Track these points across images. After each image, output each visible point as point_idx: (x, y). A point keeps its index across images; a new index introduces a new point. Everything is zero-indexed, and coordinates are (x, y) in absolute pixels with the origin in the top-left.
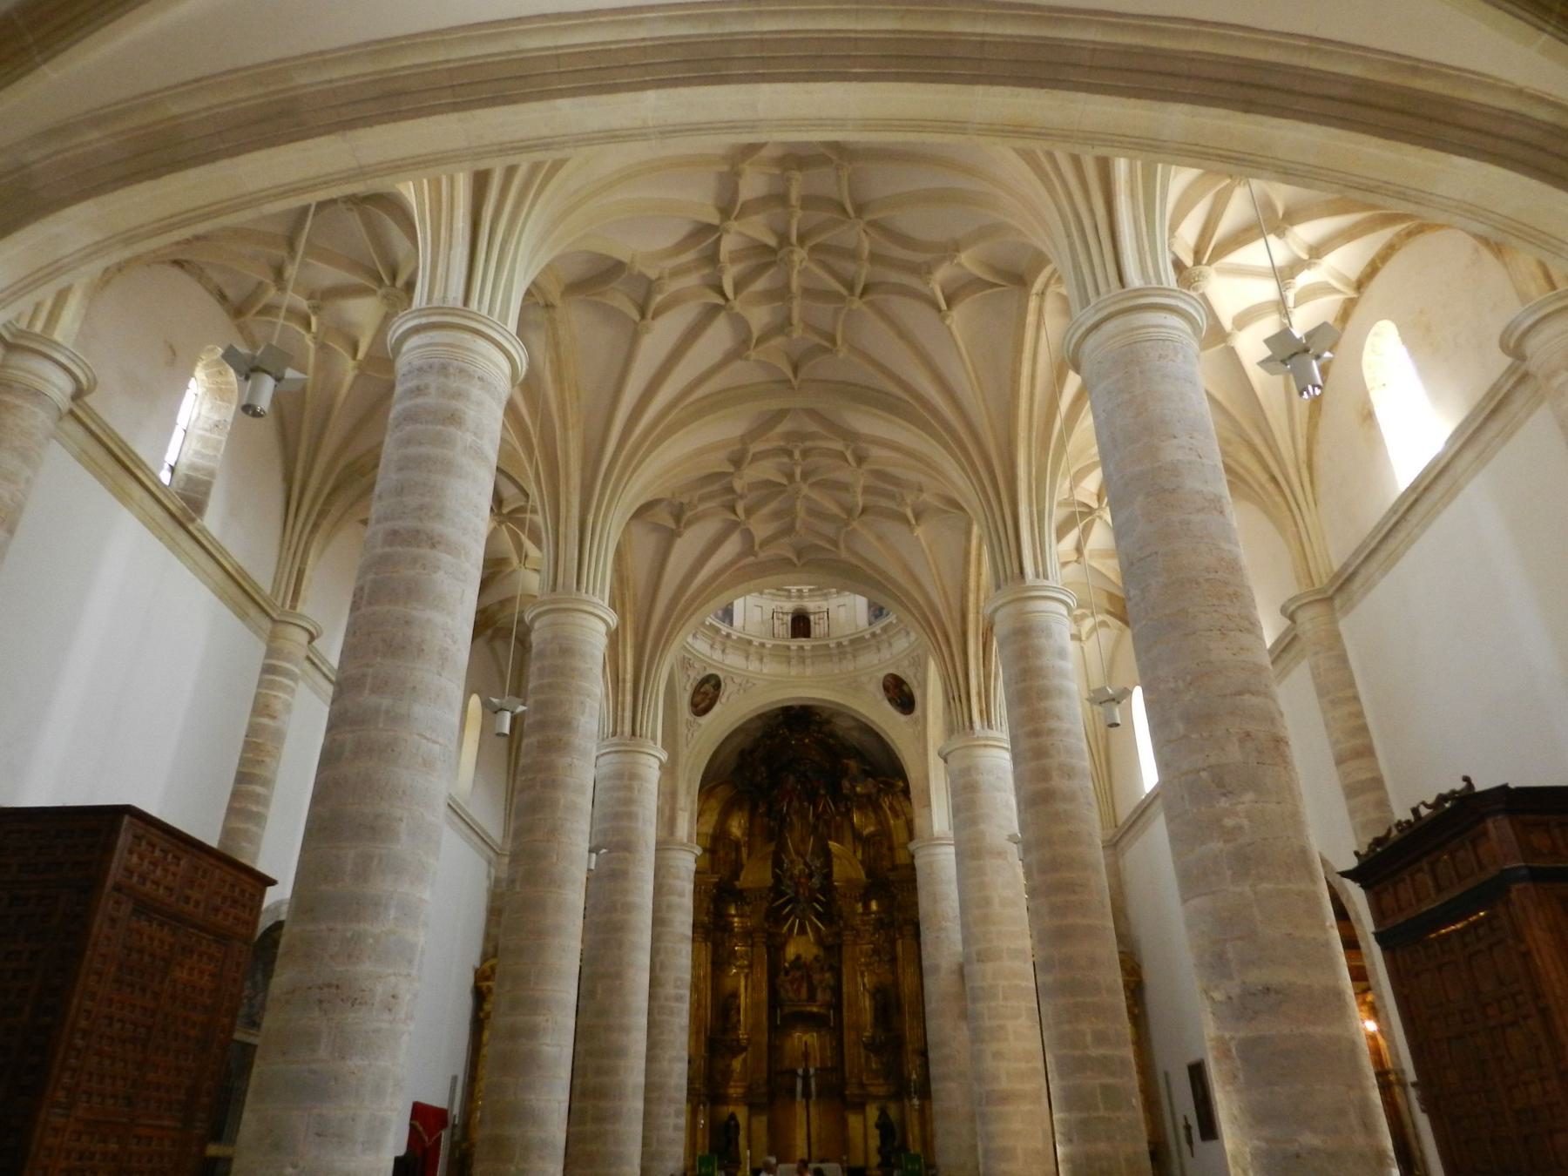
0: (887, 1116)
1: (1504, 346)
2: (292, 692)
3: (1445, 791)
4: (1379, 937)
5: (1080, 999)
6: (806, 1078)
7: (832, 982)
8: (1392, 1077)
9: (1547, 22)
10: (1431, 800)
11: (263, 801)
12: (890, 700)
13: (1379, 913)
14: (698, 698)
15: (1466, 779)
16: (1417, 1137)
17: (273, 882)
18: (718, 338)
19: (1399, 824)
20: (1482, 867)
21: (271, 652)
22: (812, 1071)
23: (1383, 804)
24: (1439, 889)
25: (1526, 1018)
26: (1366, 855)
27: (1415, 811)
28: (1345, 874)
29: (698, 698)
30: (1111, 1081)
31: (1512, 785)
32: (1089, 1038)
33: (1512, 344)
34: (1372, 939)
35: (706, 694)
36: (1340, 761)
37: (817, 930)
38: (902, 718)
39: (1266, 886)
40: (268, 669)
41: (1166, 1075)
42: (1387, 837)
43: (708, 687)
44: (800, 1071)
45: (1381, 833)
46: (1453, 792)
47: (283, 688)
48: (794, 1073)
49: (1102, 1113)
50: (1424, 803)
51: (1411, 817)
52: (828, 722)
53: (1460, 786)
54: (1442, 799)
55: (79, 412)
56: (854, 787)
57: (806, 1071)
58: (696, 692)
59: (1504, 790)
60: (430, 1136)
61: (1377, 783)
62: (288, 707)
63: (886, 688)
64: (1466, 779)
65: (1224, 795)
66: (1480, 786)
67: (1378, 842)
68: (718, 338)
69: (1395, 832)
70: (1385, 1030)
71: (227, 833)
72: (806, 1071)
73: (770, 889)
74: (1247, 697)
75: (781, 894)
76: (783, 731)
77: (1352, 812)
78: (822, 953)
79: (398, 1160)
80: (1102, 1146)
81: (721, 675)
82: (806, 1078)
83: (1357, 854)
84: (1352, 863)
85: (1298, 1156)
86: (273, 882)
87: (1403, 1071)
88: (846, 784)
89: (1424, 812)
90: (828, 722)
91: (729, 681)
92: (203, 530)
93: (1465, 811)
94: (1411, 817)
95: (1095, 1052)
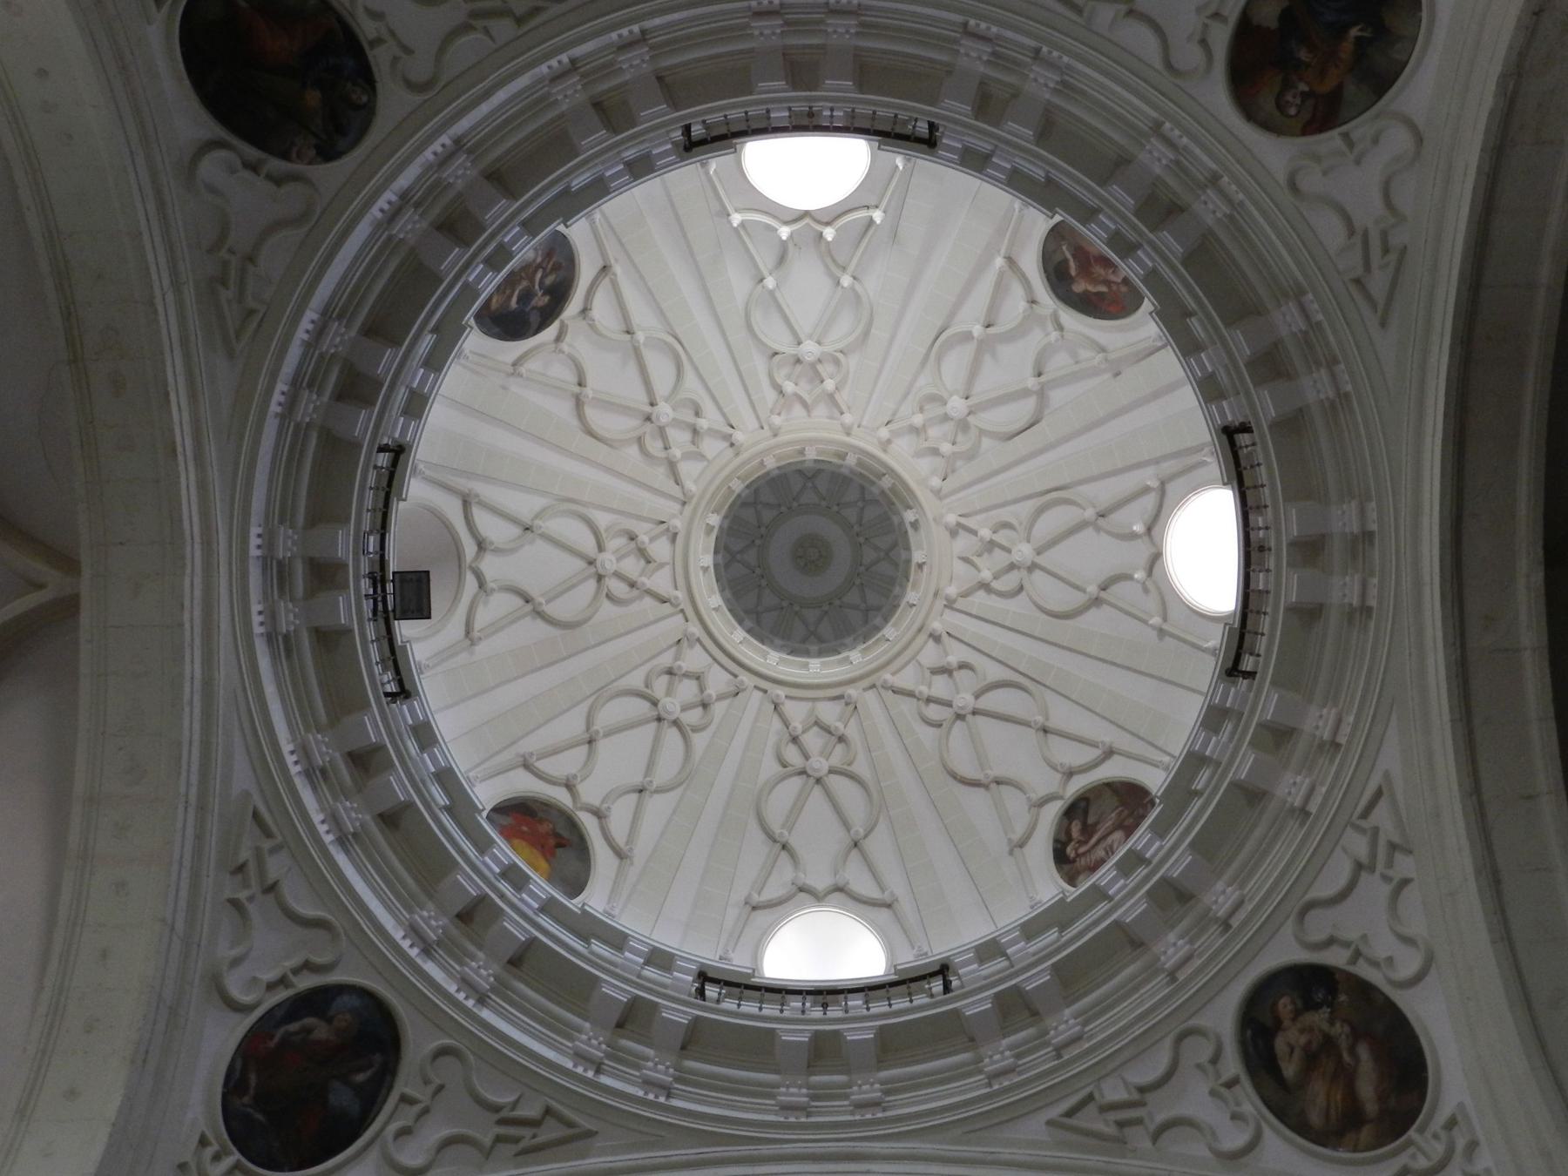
12: (1381, 81)
29: (1319, 1098)
35: (1319, 1054)
43: (1289, 1043)
63: (1324, 115)
81: (1285, 952)
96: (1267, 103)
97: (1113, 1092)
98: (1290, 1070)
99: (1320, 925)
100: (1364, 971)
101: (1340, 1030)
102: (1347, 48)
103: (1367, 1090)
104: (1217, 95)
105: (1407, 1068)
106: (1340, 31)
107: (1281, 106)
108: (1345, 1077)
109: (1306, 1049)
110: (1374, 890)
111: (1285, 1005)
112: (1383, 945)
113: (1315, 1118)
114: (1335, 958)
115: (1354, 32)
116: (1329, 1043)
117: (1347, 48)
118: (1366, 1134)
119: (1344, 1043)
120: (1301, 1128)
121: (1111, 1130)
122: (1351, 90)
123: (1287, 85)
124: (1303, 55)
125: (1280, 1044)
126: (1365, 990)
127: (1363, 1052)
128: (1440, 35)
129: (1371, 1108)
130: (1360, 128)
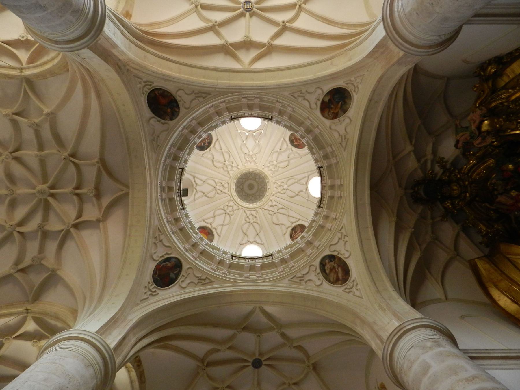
12: (345, 111)
29: (332, 276)
35: (332, 269)
43: (328, 267)
57: (41, 147)
63: (335, 116)
91: (333, 248)
96: (326, 114)
97: (299, 275)
98: (328, 272)
99: (333, 248)
100: (340, 256)
101: (336, 265)
102: (339, 105)
103: (340, 275)
104: (318, 112)
105: (347, 272)
106: (338, 103)
107: (328, 115)
108: (337, 273)
109: (330, 268)
110: (342, 242)
111: (327, 261)
112: (343, 251)
113: (332, 280)
114: (335, 253)
115: (341, 103)
116: (334, 267)
117: (339, 105)
118: (340, 282)
119: (336, 267)
120: (329, 281)
121: (299, 281)
122: (340, 112)
123: (329, 111)
124: (332, 106)
125: (326, 267)
126: (340, 259)
127: (340, 269)
128: (355, 103)
129: (341, 278)
130: (341, 118)
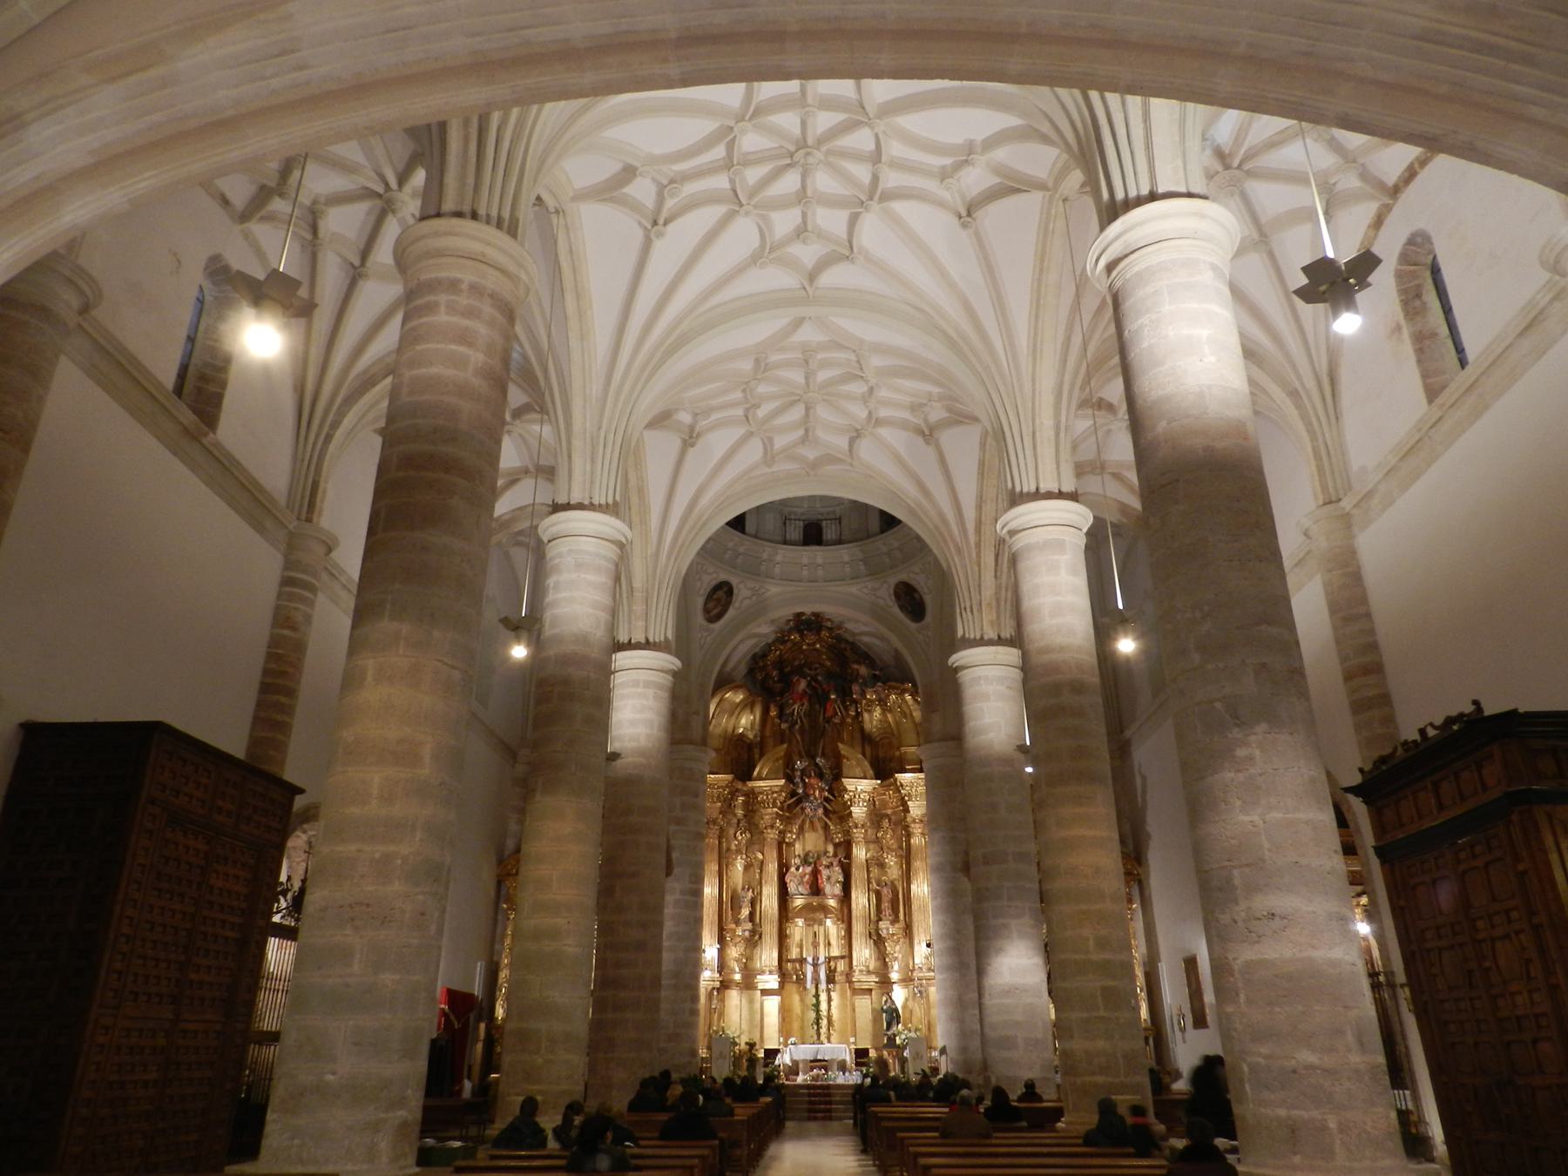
0: (906, 947)
1: (1543, 264)
2: (311, 604)
3: (1454, 713)
4: (1379, 851)
5: (1083, 907)
6: (815, 965)
7: (841, 878)
8: (1382, 978)
9: (665, 60)
10: (1439, 721)
11: (289, 710)
12: (901, 607)
13: (1379, 828)
14: (711, 605)
15: (1476, 703)
16: (1408, 1055)
17: (301, 791)
18: (742, 236)
19: (1405, 743)
20: (1485, 788)
21: (289, 564)
22: (822, 959)
23: (1390, 720)
24: (1441, 807)
25: (1517, 933)
26: (1370, 772)
27: (1422, 732)
28: (1348, 790)
30: (1111, 983)
31: (1521, 710)
32: (1091, 943)
33: (1552, 261)
34: (1371, 853)
35: (719, 600)
36: (1348, 677)
37: (826, 827)
38: (913, 625)
39: (1277, 815)
40: (287, 582)
41: (1144, 778)
42: (1392, 755)
43: (720, 594)
44: (810, 960)
45: (1387, 751)
46: (1462, 715)
47: (303, 600)
48: (802, 961)
49: (1102, 1013)
50: (1431, 724)
51: (1416, 736)
52: (839, 627)
53: (1469, 708)
54: (1450, 721)
55: (85, 325)
56: (863, 694)
57: (816, 959)
58: (709, 597)
59: (1512, 715)
60: (458, 1020)
61: (1385, 699)
62: (308, 619)
64: (1476, 703)
65: (1237, 725)
66: (1489, 711)
67: (1383, 760)
68: (742, 236)
69: (1400, 751)
70: (1380, 936)
71: (254, 743)
72: (816, 959)
73: (782, 788)
74: (1263, 627)
75: (793, 794)
76: (795, 637)
77: (1358, 728)
78: (831, 849)
79: (433, 1042)
80: (1101, 1044)
82: (815, 965)
83: (1361, 770)
84: (1357, 779)
85: (1294, 1072)
86: (301, 791)
87: (1392, 973)
88: (856, 688)
89: (1431, 732)
90: (839, 627)
92: (218, 445)
93: (1474, 734)
94: (1416, 736)
95: (1096, 957)
105: (719, 617)
120: (706, 603)
